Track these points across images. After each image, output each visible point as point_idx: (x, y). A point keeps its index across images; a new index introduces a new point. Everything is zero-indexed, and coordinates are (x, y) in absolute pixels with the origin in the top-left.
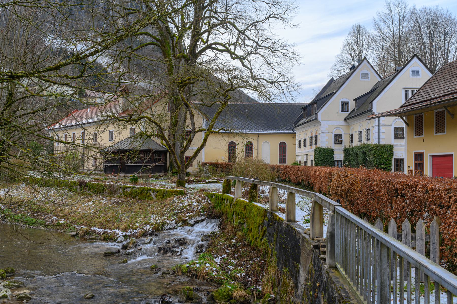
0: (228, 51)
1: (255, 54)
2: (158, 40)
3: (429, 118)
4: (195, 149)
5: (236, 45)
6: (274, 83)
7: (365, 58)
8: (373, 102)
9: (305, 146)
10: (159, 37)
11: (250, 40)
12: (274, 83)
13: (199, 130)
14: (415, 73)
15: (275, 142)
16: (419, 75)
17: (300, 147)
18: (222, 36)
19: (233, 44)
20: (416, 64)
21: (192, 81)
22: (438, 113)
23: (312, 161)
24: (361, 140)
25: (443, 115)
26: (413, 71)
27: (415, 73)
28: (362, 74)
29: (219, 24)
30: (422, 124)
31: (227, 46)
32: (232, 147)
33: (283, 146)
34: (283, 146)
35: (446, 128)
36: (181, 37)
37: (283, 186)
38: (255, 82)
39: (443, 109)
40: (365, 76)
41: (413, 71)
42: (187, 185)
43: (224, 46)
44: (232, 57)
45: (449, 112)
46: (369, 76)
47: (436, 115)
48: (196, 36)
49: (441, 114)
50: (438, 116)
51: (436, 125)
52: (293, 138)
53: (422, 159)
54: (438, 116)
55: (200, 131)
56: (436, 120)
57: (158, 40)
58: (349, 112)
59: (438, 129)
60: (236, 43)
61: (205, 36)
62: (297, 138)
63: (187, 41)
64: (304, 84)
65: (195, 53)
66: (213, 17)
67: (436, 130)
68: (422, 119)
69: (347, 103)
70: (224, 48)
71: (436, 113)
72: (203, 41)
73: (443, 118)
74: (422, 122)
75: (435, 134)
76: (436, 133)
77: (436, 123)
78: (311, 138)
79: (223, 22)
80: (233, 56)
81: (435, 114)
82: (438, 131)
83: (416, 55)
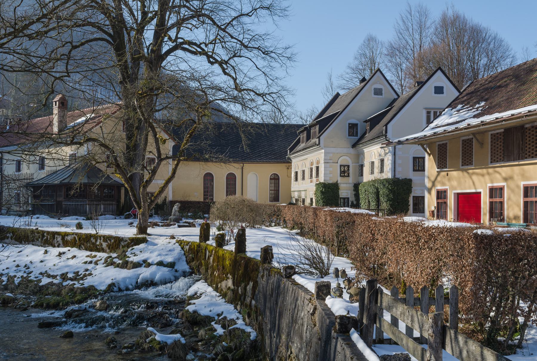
0: (204, 53)
1: (240, 56)
2: (109, 35)
3: (455, 151)
4: (162, 182)
5: (215, 44)
6: (265, 95)
7: (379, 70)
8: (388, 126)
9: (303, 178)
10: (111, 31)
12: (265, 95)
13: (167, 157)
14: (439, 90)
15: (267, 170)
16: (443, 93)
17: (296, 179)
18: (197, 33)
19: (211, 43)
20: (439, 79)
21: (156, 92)
22: (465, 142)
23: (312, 199)
24: (372, 172)
25: (470, 144)
26: (436, 88)
27: (439, 90)
28: (375, 89)
29: (192, 17)
30: (446, 154)
31: (203, 46)
32: (209, 178)
33: (275, 179)
34: (275, 179)
35: (473, 160)
36: (141, 30)
37: (279, 315)
38: (239, 93)
39: (471, 137)
40: (378, 92)
41: (436, 88)
42: (150, 230)
43: (199, 46)
44: (210, 62)
45: (477, 140)
46: (383, 92)
47: (463, 144)
48: (161, 32)
49: (468, 143)
50: (465, 145)
51: (463, 156)
52: (288, 168)
53: (445, 197)
54: (465, 148)
55: (167, 158)
56: (463, 150)
57: (109, 35)
58: (359, 137)
59: (465, 160)
60: (215, 40)
61: (172, 33)
62: (293, 169)
63: (149, 35)
64: (302, 105)
66: (185, 6)
67: (462, 162)
68: (446, 149)
69: (356, 125)
70: (199, 50)
71: (463, 140)
72: (170, 38)
73: (470, 147)
74: (446, 152)
75: (461, 167)
76: (462, 165)
77: (463, 153)
78: (311, 169)
79: (198, 14)
80: (211, 60)
81: (461, 143)
82: (465, 164)
83: (440, 68)
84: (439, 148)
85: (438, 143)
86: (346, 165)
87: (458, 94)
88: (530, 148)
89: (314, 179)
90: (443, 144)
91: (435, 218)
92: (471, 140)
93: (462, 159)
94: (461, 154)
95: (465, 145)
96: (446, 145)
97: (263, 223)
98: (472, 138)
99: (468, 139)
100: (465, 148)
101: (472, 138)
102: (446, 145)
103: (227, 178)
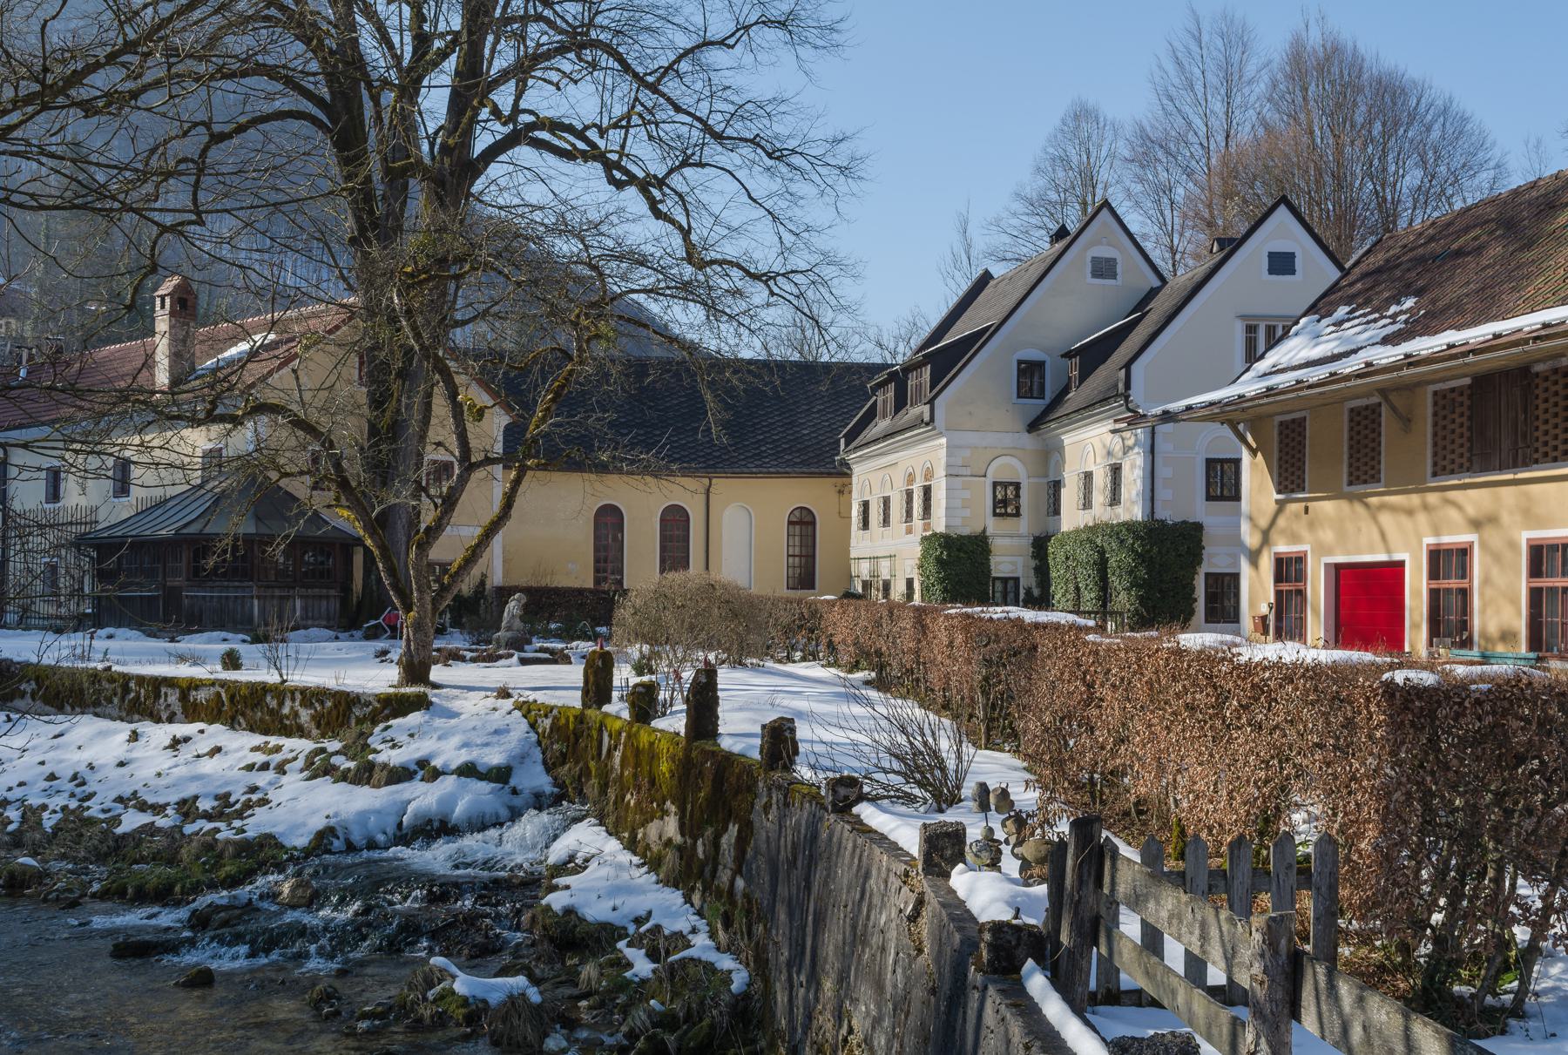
0: (594, 154)
1: (701, 165)
2: (318, 101)
3: (1329, 440)
4: (472, 533)
5: (627, 128)
6: (774, 278)
7: (1106, 204)
8: (1134, 367)
9: (886, 521)
10: (324, 92)
11: (673, 124)
12: (774, 278)
13: (487, 458)
14: (1282, 263)
15: (779, 496)
16: (1293, 272)
17: (865, 524)
18: (575, 98)
19: (616, 126)
20: (1282, 232)
21: (455, 270)
22: (1359, 414)
23: (910, 583)
24: (1087, 504)
25: (1373, 421)
26: (1273, 256)
27: (1282, 263)
28: (1095, 260)
29: (561, 50)
30: (1302, 451)
31: (592, 134)
32: (609, 521)
33: (803, 522)
34: (803, 522)
35: (1383, 466)
36: (410, 87)
38: (698, 271)
39: (1375, 399)
40: (1103, 269)
41: (1273, 256)
42: (437, 673)
43: (581, 135)
44: (612, 181)
45: (1394, 409)
46: (1119, 270)
47: (1351, 420)
48: (469, 95)
49: (1366, 418)
50: (1359, 424)
51: (1351, 456)
52: (841, 492)
53: (1301, 576)
54: (1359, 433)
55: (488, 461)
56: (1351, 438)
57: (318, 101)
58: (1048, 400)
59: (1358, 469)
60: (628, 116)
61: (504, 97)
62: (855, 494)
63: (435, 102)
64: (883, 307)
65: (459, 169)
66: (539, 18)
67: (1350, 474)
68: (1302, 435)
69: (1040, 365)
70: (581, 145)
71: (1352, 410)
72: (496, 112)
73: (1373, 431)
74: (1302, 444)
75: (1347, 489)
76: (1350, 483)
77: (1351, 447)
78: (909, 494)
79: (577, 41)
80: (617, 175)
81: (1346, 417)
82: (1358, 478)
83: (1284, 200)
84: (1280, 433)
85: (1278, 419)
86: (1011, 484)
87: (1338, 274)
88: (1546, 433)
89: (917, 523)
90: (1293, 421)
91: (1271, 637)
92: (1374, 410)
93: (1350, 465)
94: (1346, 449)
95: (1359, 424)
96: (1301, 423)
97: (767, 651)
98: (1380, 404)
99: (1367, 407)
100: (1359, 433)
101: (1380, 404)
102: (1301, 423)
103: (662, 520)
